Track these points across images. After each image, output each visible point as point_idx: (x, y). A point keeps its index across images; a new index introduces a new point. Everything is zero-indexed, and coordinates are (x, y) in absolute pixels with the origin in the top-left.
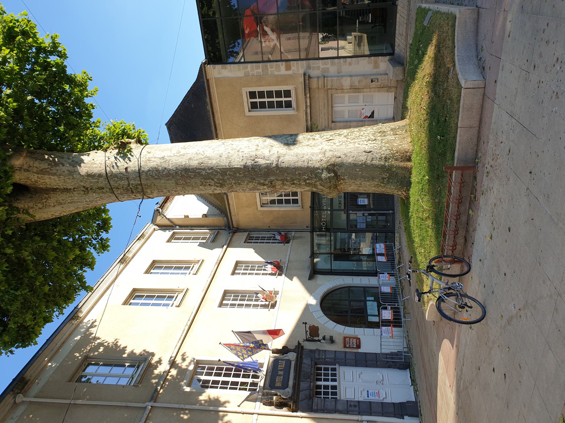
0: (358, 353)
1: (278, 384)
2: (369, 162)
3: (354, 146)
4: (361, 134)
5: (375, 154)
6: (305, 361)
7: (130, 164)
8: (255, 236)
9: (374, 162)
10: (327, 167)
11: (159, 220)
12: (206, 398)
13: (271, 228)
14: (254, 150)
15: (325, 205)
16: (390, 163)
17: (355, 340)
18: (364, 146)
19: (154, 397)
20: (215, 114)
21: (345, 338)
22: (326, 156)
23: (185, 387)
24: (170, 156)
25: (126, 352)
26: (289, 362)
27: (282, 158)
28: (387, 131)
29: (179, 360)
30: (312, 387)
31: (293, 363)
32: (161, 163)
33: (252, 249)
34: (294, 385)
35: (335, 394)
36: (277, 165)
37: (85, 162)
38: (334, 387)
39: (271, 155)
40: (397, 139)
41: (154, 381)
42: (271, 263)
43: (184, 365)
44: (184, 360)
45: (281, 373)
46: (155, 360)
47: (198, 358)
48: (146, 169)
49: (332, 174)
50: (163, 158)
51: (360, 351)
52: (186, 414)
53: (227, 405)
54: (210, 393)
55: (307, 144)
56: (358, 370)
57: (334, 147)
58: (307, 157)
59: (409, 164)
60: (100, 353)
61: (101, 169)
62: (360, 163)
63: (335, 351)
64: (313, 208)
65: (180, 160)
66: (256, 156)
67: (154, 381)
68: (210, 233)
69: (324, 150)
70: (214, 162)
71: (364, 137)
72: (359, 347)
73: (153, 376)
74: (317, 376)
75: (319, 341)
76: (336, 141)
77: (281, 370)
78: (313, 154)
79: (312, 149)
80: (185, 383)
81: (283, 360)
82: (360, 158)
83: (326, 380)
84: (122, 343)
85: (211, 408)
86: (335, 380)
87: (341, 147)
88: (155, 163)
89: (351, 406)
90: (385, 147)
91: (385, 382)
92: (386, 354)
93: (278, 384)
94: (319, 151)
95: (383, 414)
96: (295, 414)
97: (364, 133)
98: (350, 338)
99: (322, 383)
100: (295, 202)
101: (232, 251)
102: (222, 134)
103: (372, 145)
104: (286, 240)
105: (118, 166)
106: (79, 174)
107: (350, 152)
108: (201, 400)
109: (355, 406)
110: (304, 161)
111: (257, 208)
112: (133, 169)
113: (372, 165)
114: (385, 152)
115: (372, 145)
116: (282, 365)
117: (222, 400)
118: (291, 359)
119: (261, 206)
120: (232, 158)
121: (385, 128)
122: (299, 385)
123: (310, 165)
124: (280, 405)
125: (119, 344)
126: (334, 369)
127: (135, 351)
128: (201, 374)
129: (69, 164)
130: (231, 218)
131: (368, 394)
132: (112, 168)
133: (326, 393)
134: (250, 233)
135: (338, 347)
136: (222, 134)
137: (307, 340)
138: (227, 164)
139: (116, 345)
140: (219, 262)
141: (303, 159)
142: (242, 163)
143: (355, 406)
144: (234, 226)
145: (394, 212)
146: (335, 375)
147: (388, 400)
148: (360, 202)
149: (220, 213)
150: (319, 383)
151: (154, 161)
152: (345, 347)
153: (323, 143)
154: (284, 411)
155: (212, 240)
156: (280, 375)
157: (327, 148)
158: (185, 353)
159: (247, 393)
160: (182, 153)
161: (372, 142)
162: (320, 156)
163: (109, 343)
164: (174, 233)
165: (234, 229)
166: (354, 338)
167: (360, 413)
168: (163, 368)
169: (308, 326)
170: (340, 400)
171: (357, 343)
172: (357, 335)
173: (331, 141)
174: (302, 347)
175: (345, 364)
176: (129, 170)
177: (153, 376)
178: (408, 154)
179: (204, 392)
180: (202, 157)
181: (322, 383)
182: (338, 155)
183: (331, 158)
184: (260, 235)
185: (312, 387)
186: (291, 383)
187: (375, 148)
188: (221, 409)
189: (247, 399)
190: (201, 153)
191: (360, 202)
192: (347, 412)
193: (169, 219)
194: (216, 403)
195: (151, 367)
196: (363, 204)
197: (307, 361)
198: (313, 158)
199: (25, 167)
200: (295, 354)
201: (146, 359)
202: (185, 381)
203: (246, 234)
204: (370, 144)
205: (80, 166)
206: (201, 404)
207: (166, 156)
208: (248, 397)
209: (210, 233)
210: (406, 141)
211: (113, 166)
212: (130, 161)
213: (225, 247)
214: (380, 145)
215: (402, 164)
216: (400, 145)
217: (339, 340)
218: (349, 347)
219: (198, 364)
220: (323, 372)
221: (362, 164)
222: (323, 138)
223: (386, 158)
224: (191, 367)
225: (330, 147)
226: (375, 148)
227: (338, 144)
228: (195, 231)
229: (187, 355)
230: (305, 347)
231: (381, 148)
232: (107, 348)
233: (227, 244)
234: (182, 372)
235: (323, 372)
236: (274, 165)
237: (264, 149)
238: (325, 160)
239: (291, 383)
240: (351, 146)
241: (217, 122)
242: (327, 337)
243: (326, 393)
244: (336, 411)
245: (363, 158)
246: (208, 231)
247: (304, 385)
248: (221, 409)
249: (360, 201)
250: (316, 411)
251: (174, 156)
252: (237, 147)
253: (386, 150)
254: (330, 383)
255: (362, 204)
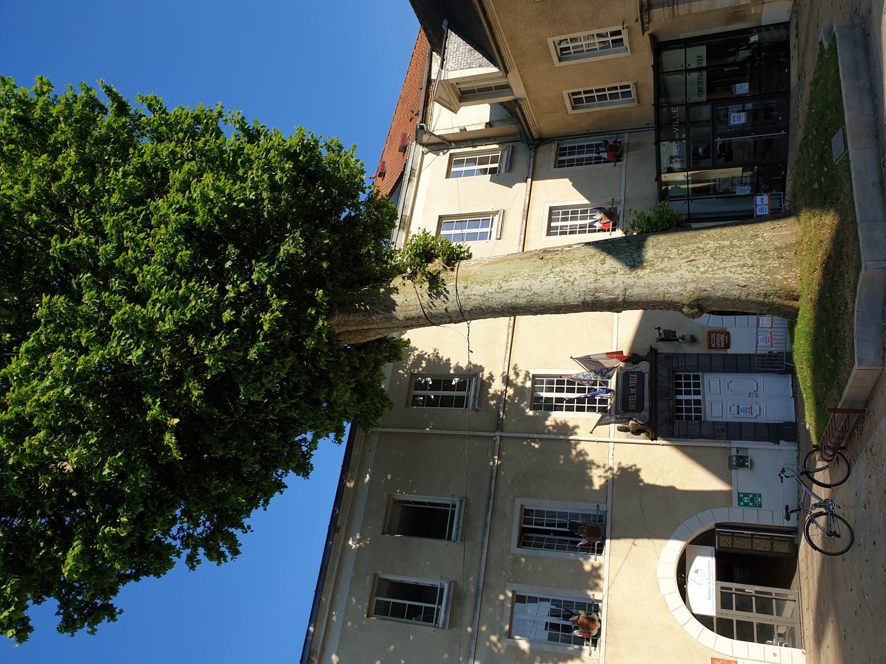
0: (727, 354)
1: (632, 407)
2: (743, 297)
3: (723, 275)
4: (733, 253)
5: (751, 289)
6: (660, 372)
7: (449, 304)
8: (567, 146)
9: (751, 297)
10: (689, 304)
11: (425, 138)
12: (553, 423)
13: (590, 131)
14: (592, 280)
15: (677, 132)
16: (770, 300)
17: (723, 336)
18: (737, 276)
19: (499, 425)
20: (487, 9)
21: (710, 333)
22: (688, 290)
23: (527, 410)
24: (491, 293)
25: (452, 366)
26: (641, 375)
27: (630, 291)
28: (769, 251)
29: (512, 377)
30: (671, 407)
31: (647, 376)
32: (483, 301)
33: (567, 180)
34: (651, 407)
35: (698, 410)
36: (624, 300)
37: (397, 303)
38: (698, 402)
39: (616, 288)
40: (782, 266)
41: (492, 403)
42: (600, 209)
43: (519, 381)
44: (517, 375)
45: (633, 391)
46: (486, 375)
47: (533, 372)
48: (468, 308)
49: (696, 310)
50: (483, 296)
51: (730, 351)
52: (537, 443)
53: (577, 430)
54: (557, 417)
55: (662, 266)
56: (727, 377)
57: (698, 274)
58: (662, 289)
59: (795, 304)
60: (424, 368)
61: (418, 311)
62: (732, 298)
63: (698, 354)
64: (657, 105)
65: (505, 298)
66: (596, 290)
67: (492, 403)
68: (501, 148)
69: (685, 280)
70: (545, 299)
71: (737, 259)
72: (728, 346)
73: (489, 396)
74: (677, 405)
75: (677, 340)
76: (699, 263)
77: (633, 387)
78: (669, 284)
79: (668, 276)
80: (526, 405)
81: (633, 373)
82: (732, 292)
83: (688, 393)
84: (444, 355)
85: (562, 437)
86: (697, 393)
87: (707, 275)
88: (476, 302)
89: (718, 430)
90: (765, 280)
91: (759, 393)
92: (763, 355)
93: (632, 407)
94: (678, 281)
95: (756, 438)
96: (654, 442)
97: (738, 252)
98: (716, 333)
99: (683, 397)
100: (627, 94)
101: (540, 185)
102: (502, 31)
103: (748, 275)
104: (616, 153)
105: (435, 306)
106: (398, 319)
107: (720, 284)
108: (548, 426)
109: (723, 430)
110: (659, 294)
111: (567, 112)
112: (454, 309)
113: (748, 300)
114: (764, 288)
115: (748, 275)
116: (633, 382)
117: (571, 424)
118: (643, 371)
119: (573, 108)
120: (567, 293)
121: (767, 245)
122: (656, 405)
123: (666, 299)
124: (637, 432)
125: (440, 355)
126: (697, 377)
127: (460, 365)
128: (541, 390)
129: (383, 310)
130: (529, 130)
131: (738, 410)
132: (429, 309)
133: (689, 410)
134: (560, 142)
135: (701, 349)
136: (502, 31)
137: (661, 340)
138: (562, 302)
139: (437, 357)
140: (526, 213)
141: (657, 291)
142: (579, 300)
143: (723, 430)
144: (535, 138)
145: (788, 134)
146: (697, 385)
147: (762, 419)
148: (734, 121)
149: (510, 116)
150: (679, 397)
151: (475, 300)
152: (710, 347)
153: (683, 266)
154: (642, 439)
155: (508, 168)
156: (633, 395)
157: (689, 276)
158: (516, 365)
159: (598, 416)
160: (504, 288)
161: (749, 271)
162: (679, 288)
163: (429, 356)
164: (451, 155)
165: (535, 143)
166: (722, 333)
167: (729, 438)
168: (497, 386)
169: (661, 332)
170: (706, 421)
171: (725, 342)
172: (726, 328)
173: (693, 263)
174: (656, 350)
175: (711, 370)
176: (449, 310)
177: (489, 396)
178: (795, 294)
179: (550, 415)
180: (530, 294)
181: (683, 397)
182: (704, 287)
183: (693, 292)
184: (576, 143)
185: (671, 407)
186: (647, 404)
187: (752, 280)
188: (571, 438)
189: (599, 423)
190: (528, 288)
191: (734, 121)
192: (713, 437)
193: (439, 136)
194: (565, 429)
195: (485, 385)
196: (738, 122)
197: (663, 372)
198: (670, 289)
199: (342, 322)
200: (648, 364)
201: (476, 375)
202: (525, 403)
203: (554, 146)
204: (745, 273)
205: (395, 310)
206: (549, 432)
207: (487, 293)
208: (600, 421)
209: (501, 148)
210: (794, 272)
211: (430, 307)
212: (447, 299)
213: (529, 180)
214: (759, 277)
215: (787, 302)
216: (786, 279)
217: (702, 337)
218: (716, 348)
219: (535, 379)
220: (683, 389)
221: (734, 299)
222: (682, 256)
223: (765, 294)
224: (529, 384)
225: (692, 274)
226: (752, 280)
227: (702, 269)
228: (479, 148)
229: (520, 367)
230: (659, 351)
231: (759, 281)
232: (428, 361)
233: (530, 175)
234: (520, 391)
235: (683, 389)
236: (620, 300)
237: (604, 277)
238: (687, 295)
239: (647, 404)
240: (720, 274)
241: (491, 18)
242: (687, 337)
243: (689, 410)
244: (700, 436)
245: (736, 293)
246: (496, 146)
247: (662, 405)
248: (571, 438)
249: (734, 117)
250: (679, 437)
251: (496, 292)
252: (570, 277)
253: (766, 285)
254: (693, 397)
255: (737, 122)
